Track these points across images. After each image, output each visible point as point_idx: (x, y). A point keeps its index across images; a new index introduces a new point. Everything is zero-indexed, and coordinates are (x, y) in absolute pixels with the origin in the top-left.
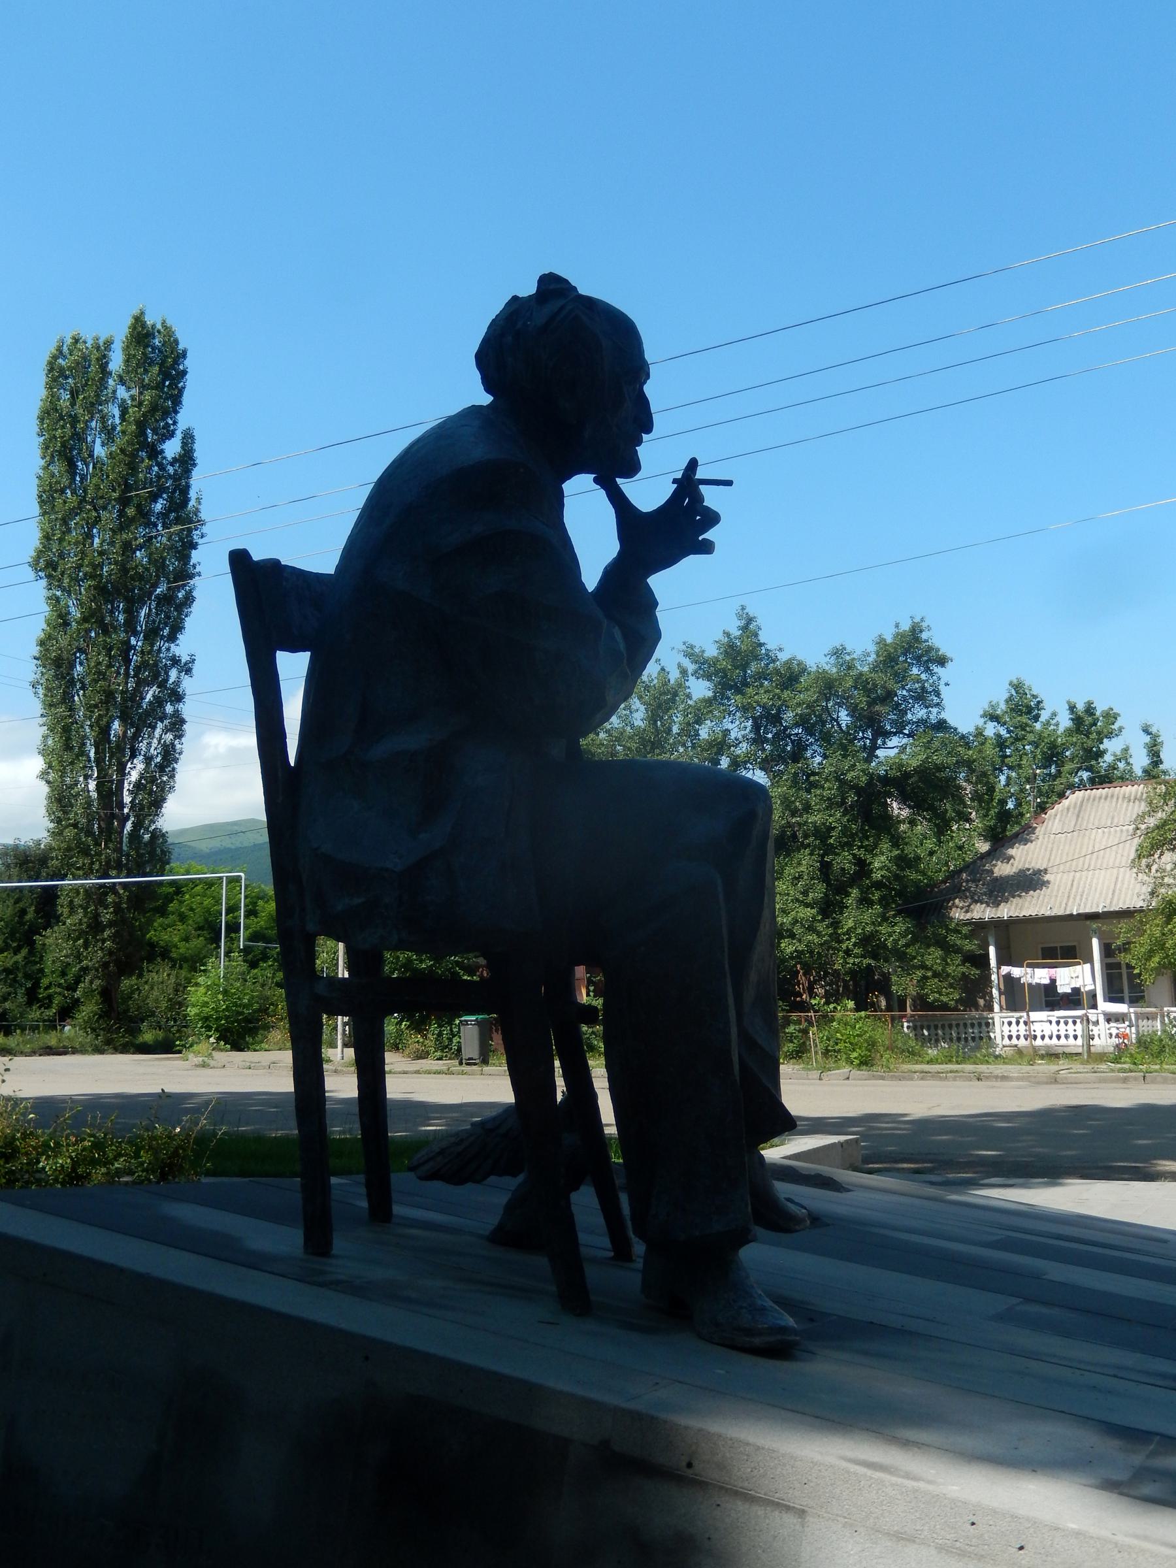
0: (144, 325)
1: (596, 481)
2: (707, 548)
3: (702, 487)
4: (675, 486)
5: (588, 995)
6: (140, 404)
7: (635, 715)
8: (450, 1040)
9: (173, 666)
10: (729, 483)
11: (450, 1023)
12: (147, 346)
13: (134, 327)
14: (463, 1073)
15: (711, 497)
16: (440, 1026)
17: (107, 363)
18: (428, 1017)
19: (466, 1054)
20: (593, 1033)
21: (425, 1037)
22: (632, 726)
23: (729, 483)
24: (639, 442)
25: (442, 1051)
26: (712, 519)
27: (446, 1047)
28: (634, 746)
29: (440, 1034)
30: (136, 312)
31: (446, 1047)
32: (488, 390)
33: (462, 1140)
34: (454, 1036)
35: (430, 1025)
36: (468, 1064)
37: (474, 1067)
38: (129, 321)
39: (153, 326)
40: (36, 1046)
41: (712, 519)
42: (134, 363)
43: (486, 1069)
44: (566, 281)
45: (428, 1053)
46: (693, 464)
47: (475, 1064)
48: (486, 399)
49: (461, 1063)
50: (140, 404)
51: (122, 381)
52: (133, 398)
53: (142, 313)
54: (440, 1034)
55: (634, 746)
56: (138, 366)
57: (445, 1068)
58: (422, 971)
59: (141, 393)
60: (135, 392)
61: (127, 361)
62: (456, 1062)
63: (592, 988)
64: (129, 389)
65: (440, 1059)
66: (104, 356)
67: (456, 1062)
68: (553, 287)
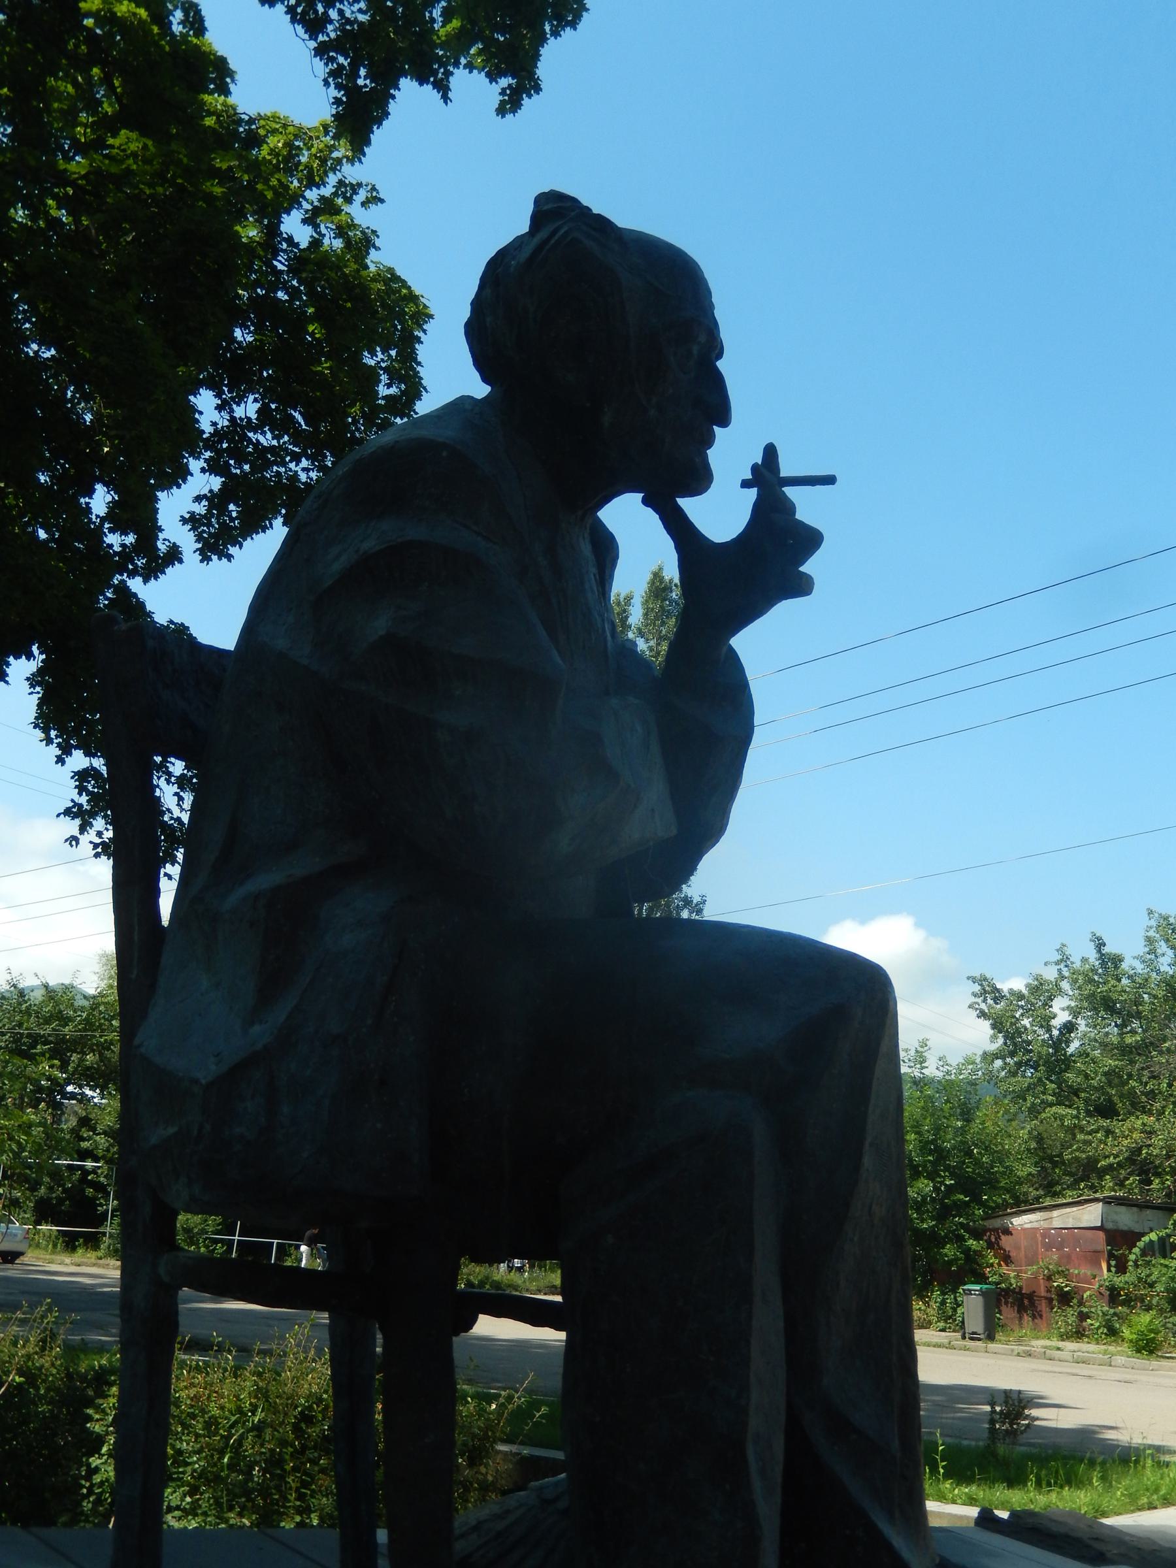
0: (662, 580)
1: (646, 502)
2: (801, 587)
3: (789, 491)
4: (753, 493)
5: (1109, 1270)
6: (658, 653)
7: (1161, 960)
8: (955, 1310)
9: (685, 906)
10: (829, 480)
11: (954, 1291)
12: (664, 599)
13: (652, 582)
14: (966, 1349)
15: (807, 506)
16: (943, 1293)
17: (627, 617)
18: (931, 1283)
19: (969, 1328)
20: (1115, 1314)
21: (927, 1304)
22: (1158, 972)
23: (829, 480)
24: (709, 441)
25: (945, 1321)
26: (810, 540)
27: (950, 1317)
28: (1161, 994)
29: (943, 1303)
30: (654, 568)
31: (950, 1317)
32: (485, 379)
33: (508, 1512)
34: (959, 1305)
35: (932, 1292)
36: (972, 1339)
37: (978, 1343)
38: (648, 577)
39: (671, 581)
40: (542, 1284)
41: (810, 540)
42: (652, 615)
43: (992, 1346)
44: (574, 200)
45: (930, 1323)
46: (770, 452)
47: (979, 1340)
48: (480, 390)
49: (964, 1337)
50: (658, 653)
51: (641, 634)
52: (651, 649)
53: (661, 569)
54: (943, 1303)
55: (1161, 994)
56: (656, 618)
57: (946, 1341)
58: (924, 1231)
59: (658, 644)
60: (652, 643)
61: (646, 615)
62: (958, 1335)
63: (1113, 1263)
64: (647, 640)
65: (943, 1330)
66: (625, 611)
67: (958, 1335)
68: (554, 210)
